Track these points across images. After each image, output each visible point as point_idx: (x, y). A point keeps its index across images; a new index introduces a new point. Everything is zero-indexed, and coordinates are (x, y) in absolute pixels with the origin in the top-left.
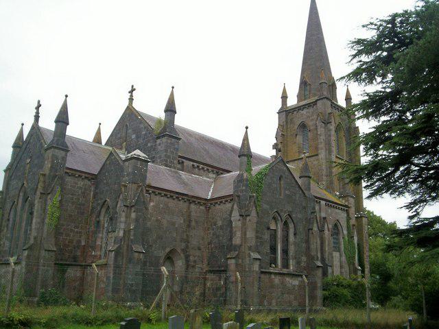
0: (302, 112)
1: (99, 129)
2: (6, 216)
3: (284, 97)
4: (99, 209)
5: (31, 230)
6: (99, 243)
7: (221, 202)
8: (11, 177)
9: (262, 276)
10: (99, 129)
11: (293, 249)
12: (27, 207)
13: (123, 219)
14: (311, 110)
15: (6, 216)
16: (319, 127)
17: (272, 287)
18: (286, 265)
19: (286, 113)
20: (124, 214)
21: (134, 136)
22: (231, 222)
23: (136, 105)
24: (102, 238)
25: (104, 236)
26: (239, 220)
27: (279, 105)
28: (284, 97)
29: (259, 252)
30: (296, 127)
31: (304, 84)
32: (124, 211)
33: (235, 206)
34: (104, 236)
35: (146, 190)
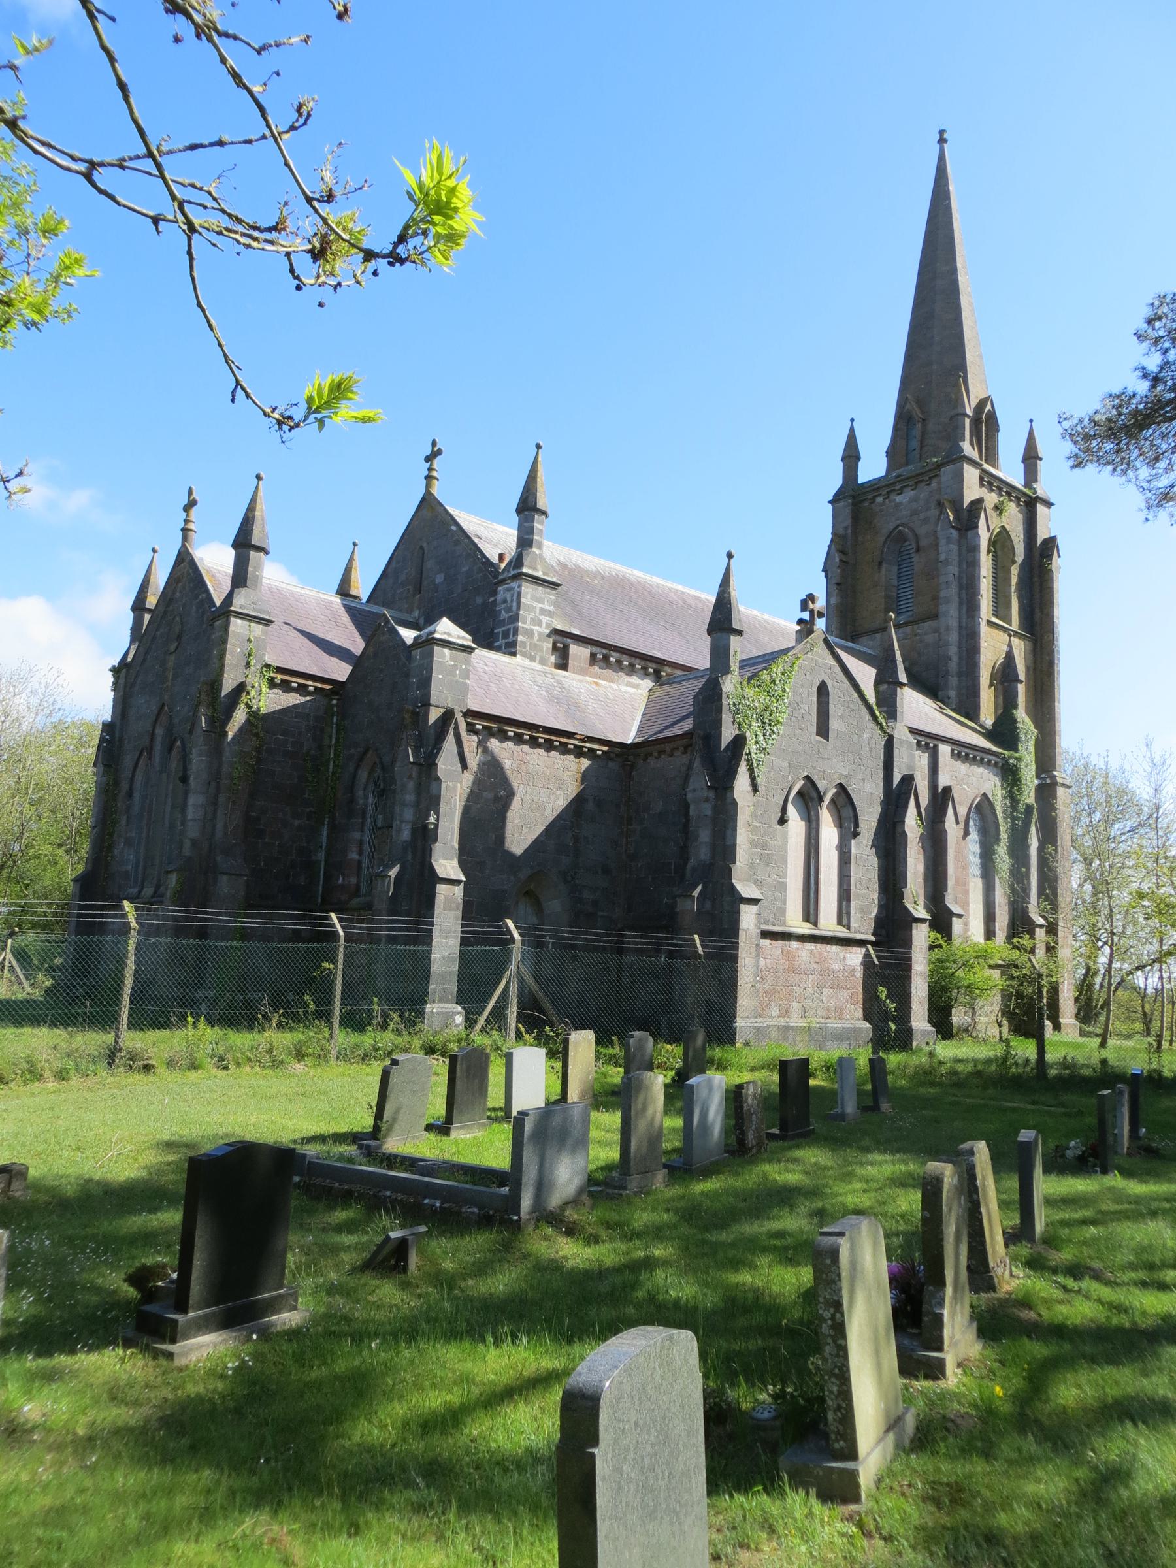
0: (898, 499)
1: (852, 430)
2: (125, 786)
3: (851, 456)
4: (352, 768)
5: (183, 823)
6: (353, 855)
7: (661, 752)
8: (133, 685)
9: (766, 943)
10: (852, 430)
11: (707, 840)
12: (174, 765)
13: (410, 798)
14: (923, 492)
15: (125, 786)
16: (942, 542)
17: (792, 970)
18: (810, 913)
19: (854, 501)
20: (411, 785)
21: (440, 578)
22: (687, 806)
23: (435, 491)
24: (361, 842)
25: (366, 838)
26: (707, 800)
27: (836, 481)
28: (851, 456)
29: (755, 882)
30: (881, 539)
31: (904, 420)
32: (410, 777)
33: (697, 764)
34: (366, 838)
35: (468, 724)
